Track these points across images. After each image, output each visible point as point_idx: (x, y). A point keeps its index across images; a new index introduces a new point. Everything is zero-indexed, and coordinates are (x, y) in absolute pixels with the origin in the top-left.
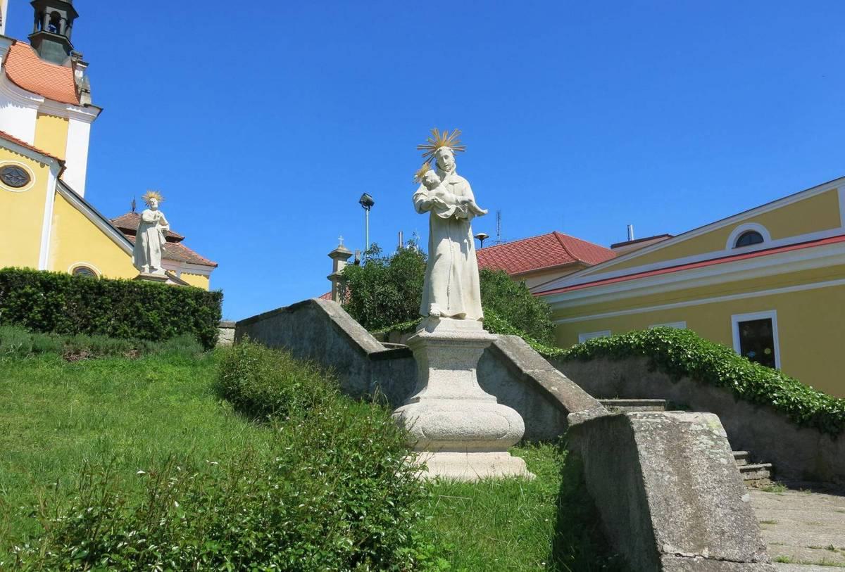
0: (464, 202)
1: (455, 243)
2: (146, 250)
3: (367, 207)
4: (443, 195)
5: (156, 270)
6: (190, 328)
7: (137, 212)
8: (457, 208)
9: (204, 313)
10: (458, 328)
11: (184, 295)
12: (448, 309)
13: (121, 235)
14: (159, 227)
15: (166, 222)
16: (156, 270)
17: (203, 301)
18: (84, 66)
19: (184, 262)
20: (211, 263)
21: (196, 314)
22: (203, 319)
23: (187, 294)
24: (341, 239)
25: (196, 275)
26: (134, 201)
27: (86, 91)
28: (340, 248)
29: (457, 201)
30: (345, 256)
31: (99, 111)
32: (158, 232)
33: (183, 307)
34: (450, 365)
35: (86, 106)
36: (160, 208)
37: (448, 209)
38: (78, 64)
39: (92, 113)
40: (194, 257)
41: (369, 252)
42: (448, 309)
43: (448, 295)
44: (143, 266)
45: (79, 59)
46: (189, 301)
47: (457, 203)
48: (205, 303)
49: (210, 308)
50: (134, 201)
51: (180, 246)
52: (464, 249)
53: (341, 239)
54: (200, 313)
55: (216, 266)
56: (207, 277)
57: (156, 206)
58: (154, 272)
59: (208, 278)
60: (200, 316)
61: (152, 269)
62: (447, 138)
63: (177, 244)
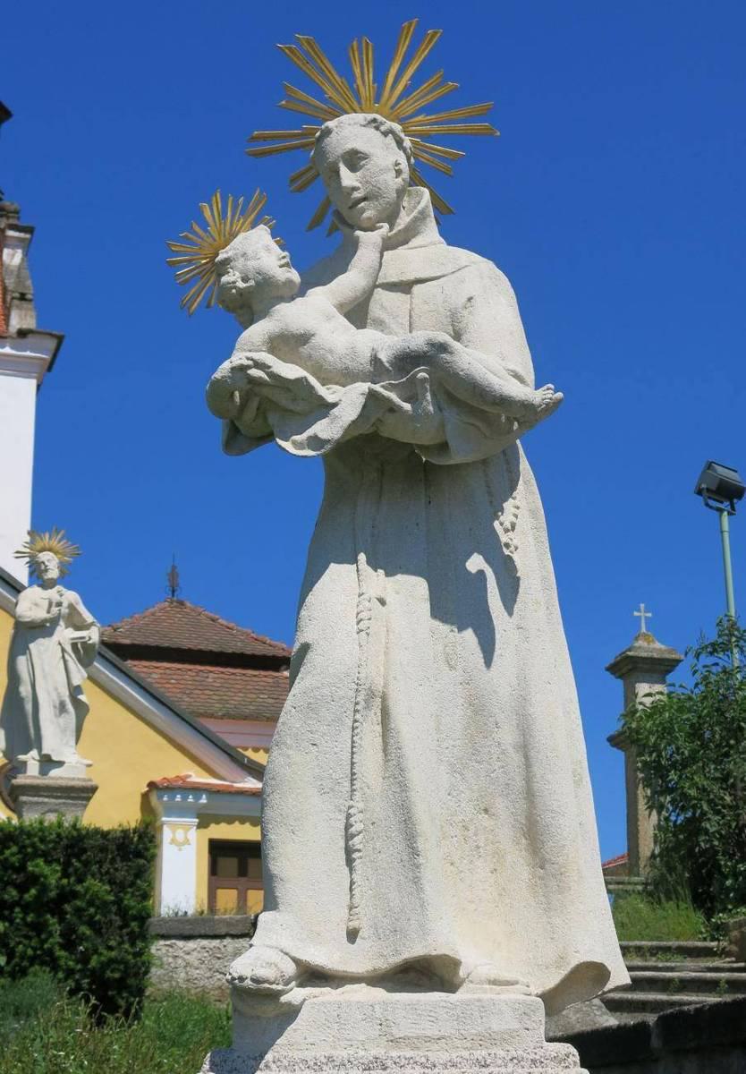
0: (407, 360)
1: (400, 578)
2: (29, 707)
3: (725, 505)
4: (304, 338)
5: (60, 764)
6: (50, 952)
7: (182, 598)
8: (372, 396)
9: (91, 903)
10: (395, 1041)
11: (22, 848)
12: (352, 935)
13: (115, 666)
14: (65, 634)
15: (89, 618)
16: (60, 764)
17: (86, 864)
18: (22, 235)
21: (67, 907)
22: (91, 923)
23: (33, 845)
24: (642, 614)
26: (174, 568)
27: (23, 297)
28: (641, 643)
29: (375, 360)
30: (659, 668)
31: (52, 344)
32: (63, 650)
33: (23, 889)
35: (22, 334)
36: (66, 579)
37: (325, 408)
38: (11, 233)
39: (36, 353)
41: (714, 649)
42: (352, 935)
43: (350, 862)
44: (22, 757)
45: (12, 221)
46: (38, 866)
47: (376, 369)
48: (95, 868)
49: (111, 882)
50: (174, 568)
52: (460, 605)
53: (642, 614)
54: (78, 903)
57: (53, 573)
58: (54, 773)
60: (79, 912)
61: (47, 763)
62: (380, 79)
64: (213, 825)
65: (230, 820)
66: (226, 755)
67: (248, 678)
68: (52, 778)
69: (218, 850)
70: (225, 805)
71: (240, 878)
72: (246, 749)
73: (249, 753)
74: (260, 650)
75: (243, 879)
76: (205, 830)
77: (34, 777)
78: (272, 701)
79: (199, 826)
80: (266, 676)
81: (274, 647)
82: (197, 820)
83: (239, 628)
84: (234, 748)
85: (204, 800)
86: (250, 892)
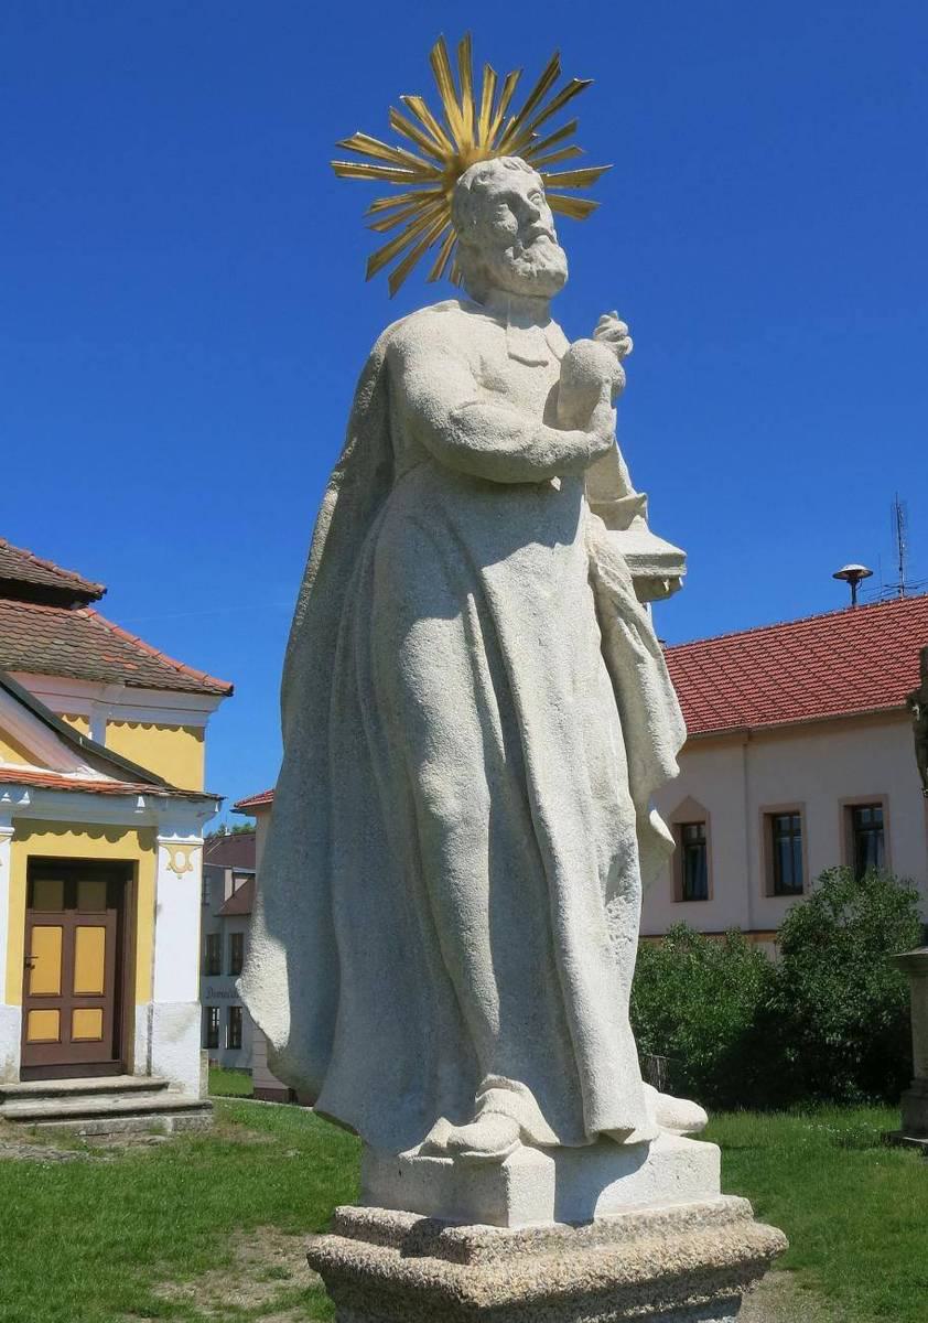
19: (114, 681)
20: (211, 681)
25: (160, 727)
34: (711, 1307)
40: (149, 664)
51: (93, 623)
55: (229, 693)
56: (198, 733)
59: (200, 738)
63: (81, 613)
64: (34, 836)
65: (59, 828)
66: (53, 734)
67: (33, 616)
68: (613, 1233)
69: (40, 870)
70: (54, 808)
71: (67, 911)
72: (73, 718)
73: (79, 726)
74: (47, 579)
75: (70, 912)
76: (23, 843)
77: (541, 1240)
78: (71, 649)
79: (14, 838)
80: (55, 614)
81: (65, 577)
82: (13, 829)
83: (13, 547)
84: (57, 717)
85: (26, 801)
86: (77, 1012)
